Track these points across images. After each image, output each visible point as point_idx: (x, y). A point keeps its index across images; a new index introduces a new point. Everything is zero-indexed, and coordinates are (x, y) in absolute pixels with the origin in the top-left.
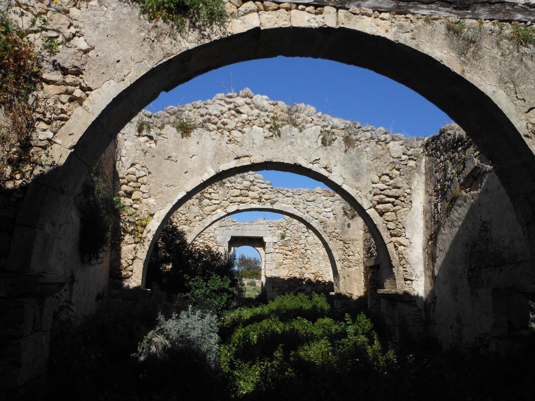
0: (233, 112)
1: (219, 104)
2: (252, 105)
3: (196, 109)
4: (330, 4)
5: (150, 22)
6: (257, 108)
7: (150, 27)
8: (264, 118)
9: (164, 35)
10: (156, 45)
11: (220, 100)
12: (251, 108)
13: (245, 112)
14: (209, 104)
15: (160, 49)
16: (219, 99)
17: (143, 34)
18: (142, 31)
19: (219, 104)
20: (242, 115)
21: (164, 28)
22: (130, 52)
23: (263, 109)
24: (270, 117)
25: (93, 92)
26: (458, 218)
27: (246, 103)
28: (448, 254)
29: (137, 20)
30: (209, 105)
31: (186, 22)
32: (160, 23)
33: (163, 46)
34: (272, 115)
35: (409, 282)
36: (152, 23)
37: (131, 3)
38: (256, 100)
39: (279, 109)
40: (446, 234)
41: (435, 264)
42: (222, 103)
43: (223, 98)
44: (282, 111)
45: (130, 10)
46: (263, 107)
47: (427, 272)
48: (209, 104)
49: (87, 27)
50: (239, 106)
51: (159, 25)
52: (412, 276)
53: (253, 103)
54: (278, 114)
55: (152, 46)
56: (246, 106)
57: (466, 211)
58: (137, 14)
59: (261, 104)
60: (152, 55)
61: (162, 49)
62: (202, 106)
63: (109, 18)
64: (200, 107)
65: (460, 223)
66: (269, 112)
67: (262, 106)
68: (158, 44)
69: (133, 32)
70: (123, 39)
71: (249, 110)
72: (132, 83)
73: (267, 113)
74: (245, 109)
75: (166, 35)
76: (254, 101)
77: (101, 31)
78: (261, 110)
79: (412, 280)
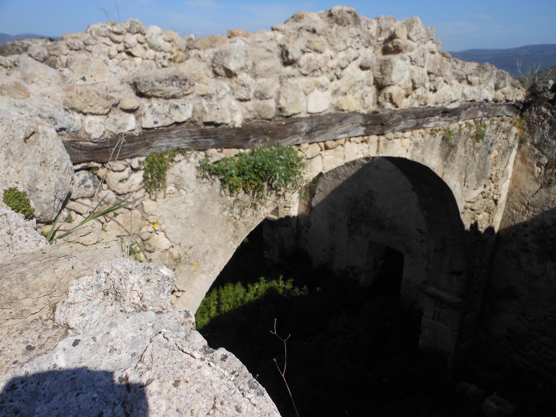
0: (124, 55)
1: (104, 43)
2: (146, 45)
3: (74, 51)
4: (375, 132)
5: (231, 197)
6: (152, 47)
7: (232, 202)
8: (160, 61)
9: (246, 209)
10: (239, 222)
11: (104, 37)
12: (145, 48)
13: (139, 55)
14: (92, 45)
15: (243, 225)
16: (103, 36)
17: (226, 213)
18: (225, 210)
19: (104, 43)
20: (135, 59)
21: (245, 200)
22: (216, 237)
23: (159, 49)
24: (166, 58)
25: (186, 294)
26: (344, 174)
27: (139, 42)
28: (329, 197)
29: (219, 198)
30: (91, 47)
31: (263, 186)
32: (241, 194)
33: (246, 220)
34: (169, 56)
35: (287, 209)
36: (233, 196)
37: (209, 177)
38: (151, 37)
39: (176, 47)
40: (328, 181)
41: (313, 199)
42: (108, 41)
43: (108, 34)
44: (180, 50)
45: (210, 187)
46: (159, 47)
47: (303, 201)
48: (92, 45)
49: (167, 222)
50: (131, 48)
51: (240, 197)
52: (290, 204)
53: (147, 42)
54: (175, 54)
55: (236, 224)
56: (139, 46)
57: (353, 172)
58: (218, 190)
59: (156, 43)
60: (236, 234)
61: (245, 224)
62: (82, 48)
63: (189, 203)
64: (80, 49)
65: (345, 179)
66: (165, 52)
67: (158, 46)
68: (241, 219)
69: (216, 214)
70: (206, 224)
71: (143, 51)
72: (221, 271)
73: (163, 54)
74: (138, 50)
75: (248, 207)
76: (149, 40)
77: (183, 222)
78: (157, 50)
79: (289, 207)
